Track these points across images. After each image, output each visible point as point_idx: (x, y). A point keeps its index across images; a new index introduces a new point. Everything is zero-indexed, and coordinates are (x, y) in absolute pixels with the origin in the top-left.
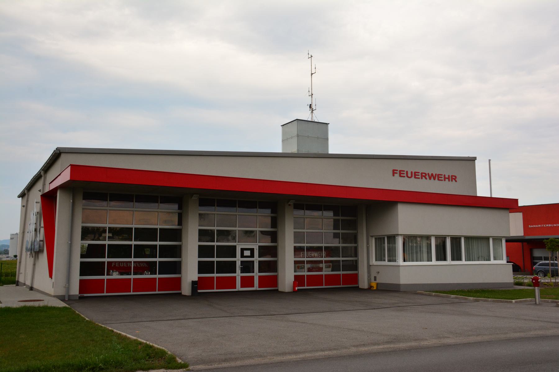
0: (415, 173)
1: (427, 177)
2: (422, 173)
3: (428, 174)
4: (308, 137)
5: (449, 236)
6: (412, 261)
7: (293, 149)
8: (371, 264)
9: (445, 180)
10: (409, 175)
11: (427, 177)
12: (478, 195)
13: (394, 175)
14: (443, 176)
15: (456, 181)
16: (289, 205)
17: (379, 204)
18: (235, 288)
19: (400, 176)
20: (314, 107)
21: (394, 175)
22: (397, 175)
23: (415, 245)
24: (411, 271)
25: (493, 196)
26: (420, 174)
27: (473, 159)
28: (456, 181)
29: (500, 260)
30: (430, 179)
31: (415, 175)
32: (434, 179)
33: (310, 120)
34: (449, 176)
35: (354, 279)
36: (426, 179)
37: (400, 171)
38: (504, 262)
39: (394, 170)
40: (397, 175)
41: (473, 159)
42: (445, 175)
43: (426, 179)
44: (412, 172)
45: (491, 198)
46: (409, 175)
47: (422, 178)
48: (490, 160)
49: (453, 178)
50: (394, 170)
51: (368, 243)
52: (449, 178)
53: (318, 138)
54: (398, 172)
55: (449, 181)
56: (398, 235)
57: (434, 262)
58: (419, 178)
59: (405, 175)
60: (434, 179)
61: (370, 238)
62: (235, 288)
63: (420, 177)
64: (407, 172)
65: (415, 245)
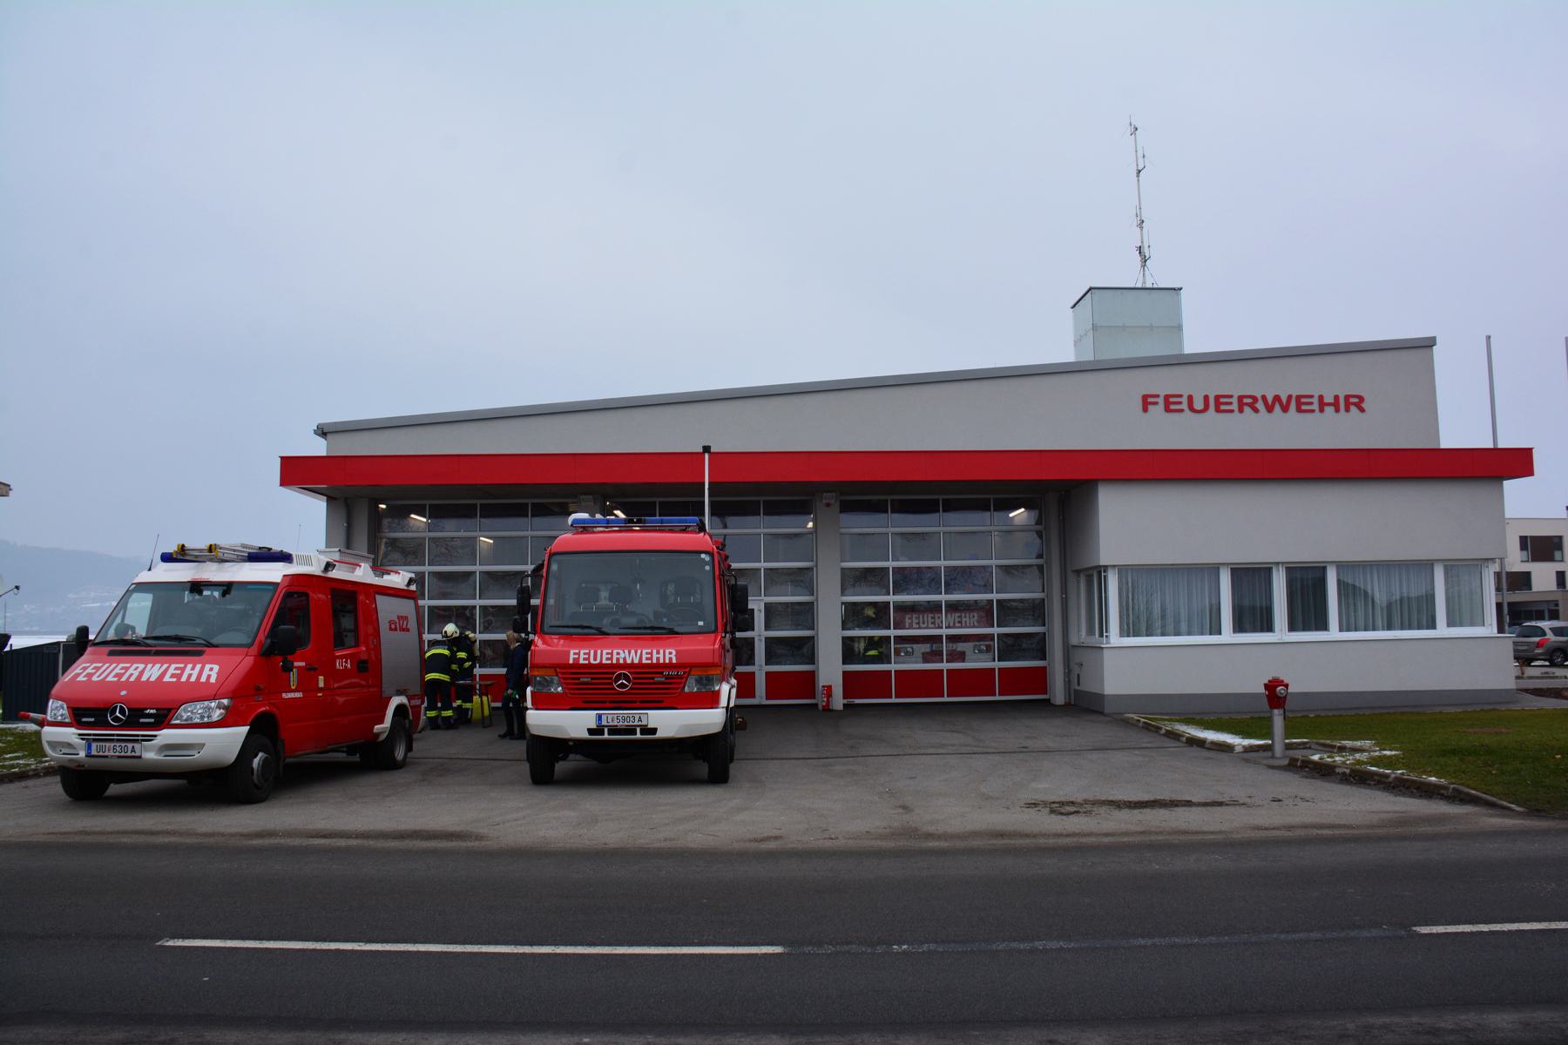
0: (1217, 398)
1: (1260, 405)
2: (1241, 398)
3: (1264, 398)
4: (1124, 327)
5: (1277, 564)
6: (1177, 634)
7: (1088, 356)
8: (1074, 640)
9: (1322, 410)
10: (1199, 405)
11: (1260, 405)
12: (1447, 442)
13: (1145, 410)
14: (1315, 401)
15: (1362, 410)
16: (828, 505)
17: (1057, 491)
18: (753, 696)
19: (1167, 409)
20: (1146, 251)
21: (1145, 410)
22: (1157, 410)
23: (1164, 596)
24: (1130, 662)
25: (1501, 445)
26: (1234, 400)
27: (1426, 345)
28: (1362, 410)
29: (1472, 624)
30: (1270, 409)
31: (1219, 403)
32: (1285, 409)
33: (1139, 285)
34: (1337, 398)
35: (1038, 679)
36: (1256, 410)
37: (1167, 397)
38: (1490, 629)
39: (1145, 397)
40: (1157, 410)
41: (1426, 345)
42: (1321, 397)
43: (1256, 410)
44: (1206, 398)
45: (1495, 450)
46: (1199, 405)
47: (1241, 410)
48: (1489, 338)
49: (1355, 402)
50: (1145, 397)
51: (1064, 589)
52: (1336, 404)
53: (1151, 327)
54: (1161, 400)
55: (1337, 410)
56: (1106, 568)
57: (1228, 635)
58: (1231, 411)
59: (1185, 406)
60: (1285, 409)
61: (1072, 578)
62: (753, 696)
63: (1235, 406)
64: (1190, 398)
65: (1164, 596)
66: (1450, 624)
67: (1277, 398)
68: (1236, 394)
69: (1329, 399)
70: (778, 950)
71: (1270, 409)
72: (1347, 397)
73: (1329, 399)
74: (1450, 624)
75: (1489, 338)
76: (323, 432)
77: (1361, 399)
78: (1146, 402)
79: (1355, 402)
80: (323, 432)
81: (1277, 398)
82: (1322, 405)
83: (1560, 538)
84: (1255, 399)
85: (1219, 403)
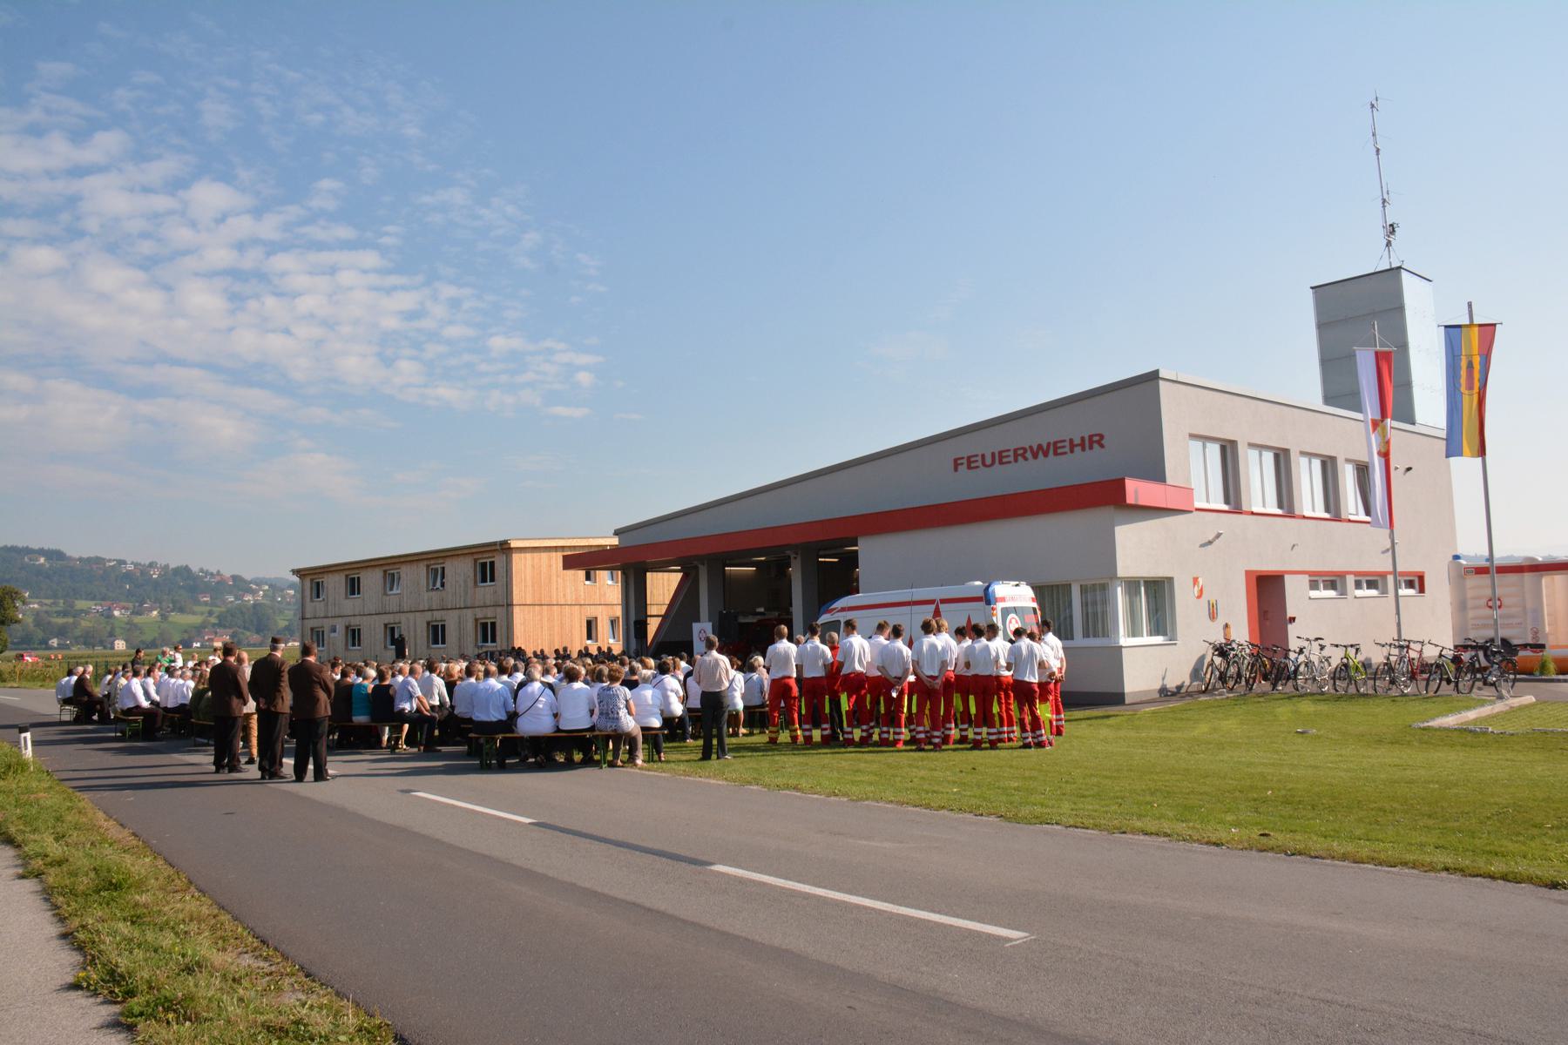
10: (989, 461)
11: (1029, 455)
25: (516, 610)
30: (1035, 456)
32: (1046, 454)
39: (956, 460)
46: (989, 461)
48: (1470, 305)
52: (1082, 445)
60: (1046, 454)
66: (1086, 635)
67: (1040, 447)
68: (1012, 447)
69: (1077, 441)
70: (827, 710)
71: (1035, 456)
72: (1091, 437)
73: (1077, 441)
74: (1086, 635)
75: (1470, 305)
76: (617, 533)
77: (1102, 437)
78: (956, 464)
79: (1095, 441)
80: (617, 533)
81: (1040, 447)
82: (1072, 446)
83: (1170, 580)
84: (1025, 450)
85: (1000, 458)
